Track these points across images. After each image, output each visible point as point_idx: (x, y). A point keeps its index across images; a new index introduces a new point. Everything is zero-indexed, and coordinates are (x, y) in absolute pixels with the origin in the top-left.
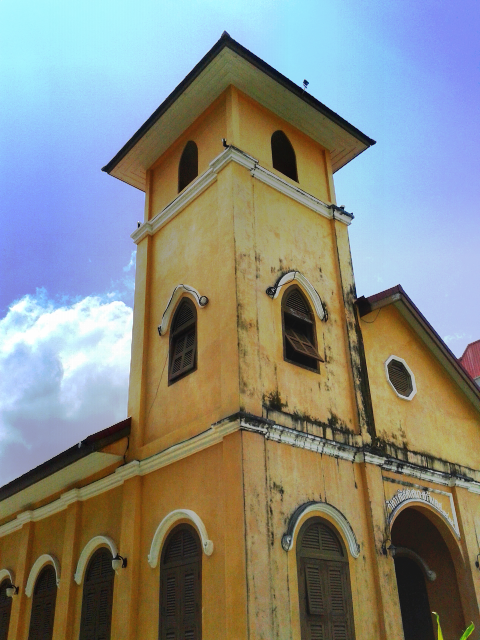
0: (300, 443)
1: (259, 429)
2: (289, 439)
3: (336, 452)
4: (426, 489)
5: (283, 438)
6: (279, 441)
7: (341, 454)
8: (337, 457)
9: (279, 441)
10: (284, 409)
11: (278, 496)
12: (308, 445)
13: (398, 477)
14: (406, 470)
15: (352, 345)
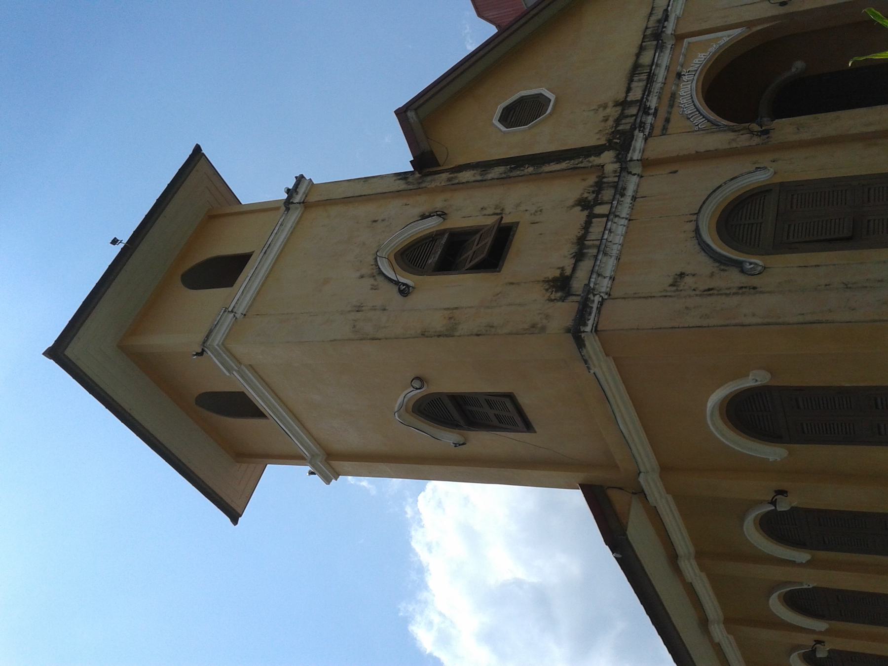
0: (615, 250)
1: (595, 306)
2: (609, 266)
3: (628, 200)
4: (679, 75)
5: (608, 272)
6: (613, 279)
7: (630, 192)
8: (634, 198)
9: (613, 279)
10: (568, 272)
11: (688, 280)
12: (618, 239)
13: (662, 114)
14: (653, 103)
15: (479, 178)
